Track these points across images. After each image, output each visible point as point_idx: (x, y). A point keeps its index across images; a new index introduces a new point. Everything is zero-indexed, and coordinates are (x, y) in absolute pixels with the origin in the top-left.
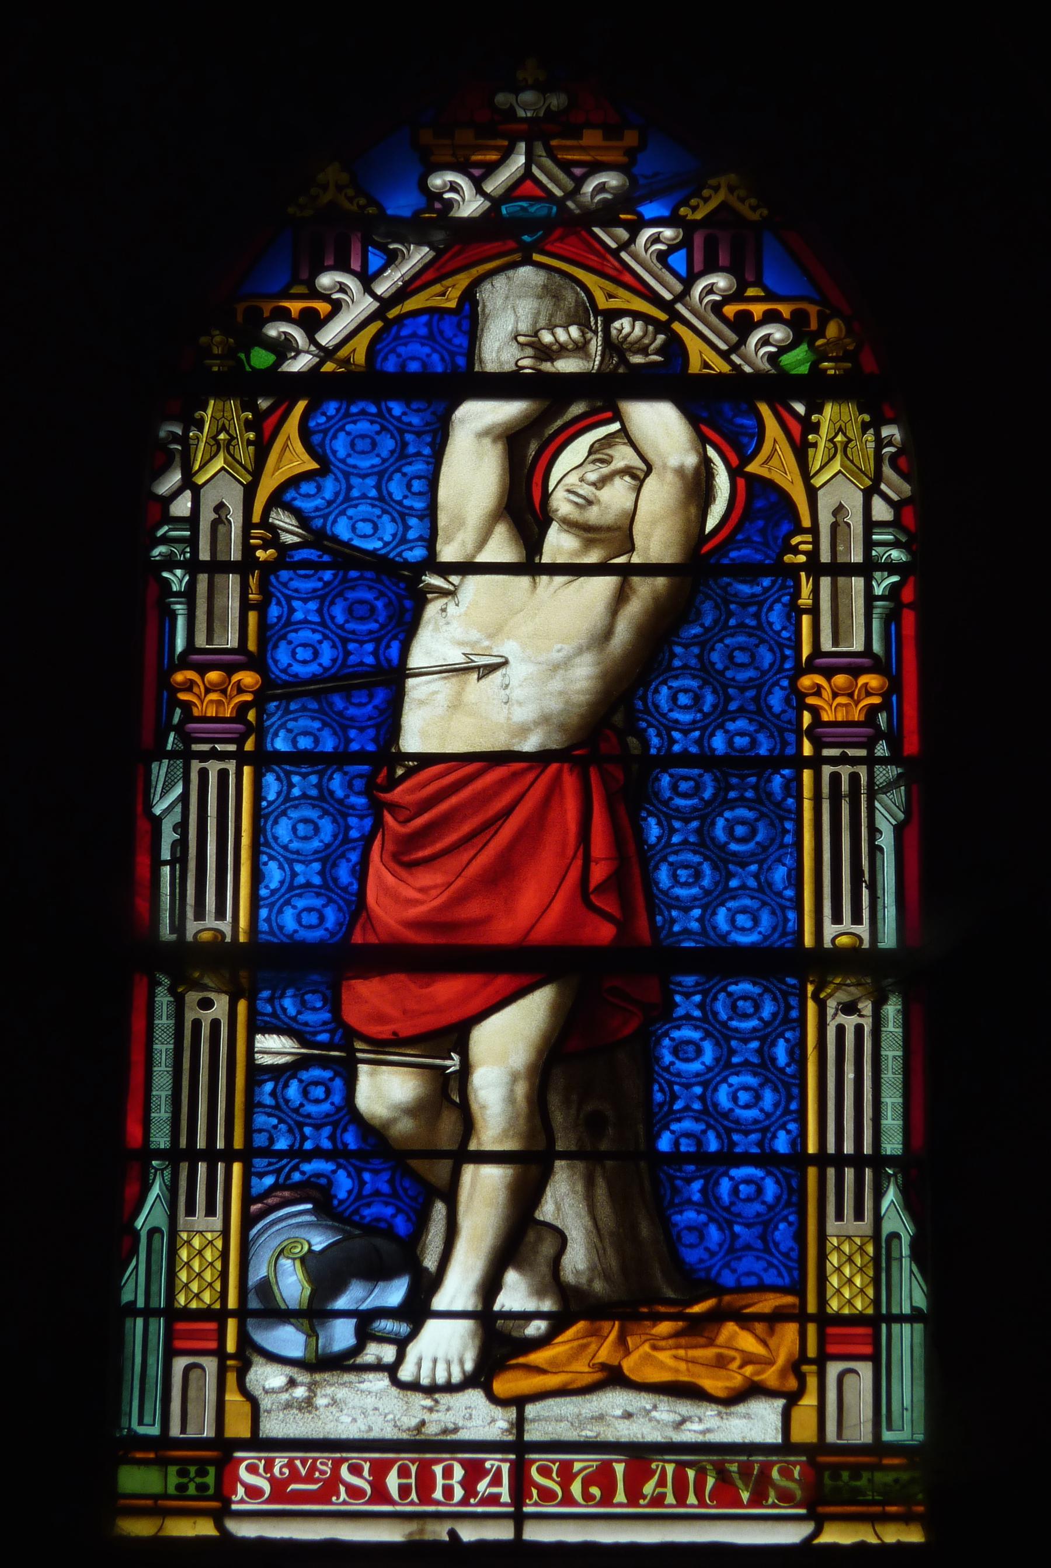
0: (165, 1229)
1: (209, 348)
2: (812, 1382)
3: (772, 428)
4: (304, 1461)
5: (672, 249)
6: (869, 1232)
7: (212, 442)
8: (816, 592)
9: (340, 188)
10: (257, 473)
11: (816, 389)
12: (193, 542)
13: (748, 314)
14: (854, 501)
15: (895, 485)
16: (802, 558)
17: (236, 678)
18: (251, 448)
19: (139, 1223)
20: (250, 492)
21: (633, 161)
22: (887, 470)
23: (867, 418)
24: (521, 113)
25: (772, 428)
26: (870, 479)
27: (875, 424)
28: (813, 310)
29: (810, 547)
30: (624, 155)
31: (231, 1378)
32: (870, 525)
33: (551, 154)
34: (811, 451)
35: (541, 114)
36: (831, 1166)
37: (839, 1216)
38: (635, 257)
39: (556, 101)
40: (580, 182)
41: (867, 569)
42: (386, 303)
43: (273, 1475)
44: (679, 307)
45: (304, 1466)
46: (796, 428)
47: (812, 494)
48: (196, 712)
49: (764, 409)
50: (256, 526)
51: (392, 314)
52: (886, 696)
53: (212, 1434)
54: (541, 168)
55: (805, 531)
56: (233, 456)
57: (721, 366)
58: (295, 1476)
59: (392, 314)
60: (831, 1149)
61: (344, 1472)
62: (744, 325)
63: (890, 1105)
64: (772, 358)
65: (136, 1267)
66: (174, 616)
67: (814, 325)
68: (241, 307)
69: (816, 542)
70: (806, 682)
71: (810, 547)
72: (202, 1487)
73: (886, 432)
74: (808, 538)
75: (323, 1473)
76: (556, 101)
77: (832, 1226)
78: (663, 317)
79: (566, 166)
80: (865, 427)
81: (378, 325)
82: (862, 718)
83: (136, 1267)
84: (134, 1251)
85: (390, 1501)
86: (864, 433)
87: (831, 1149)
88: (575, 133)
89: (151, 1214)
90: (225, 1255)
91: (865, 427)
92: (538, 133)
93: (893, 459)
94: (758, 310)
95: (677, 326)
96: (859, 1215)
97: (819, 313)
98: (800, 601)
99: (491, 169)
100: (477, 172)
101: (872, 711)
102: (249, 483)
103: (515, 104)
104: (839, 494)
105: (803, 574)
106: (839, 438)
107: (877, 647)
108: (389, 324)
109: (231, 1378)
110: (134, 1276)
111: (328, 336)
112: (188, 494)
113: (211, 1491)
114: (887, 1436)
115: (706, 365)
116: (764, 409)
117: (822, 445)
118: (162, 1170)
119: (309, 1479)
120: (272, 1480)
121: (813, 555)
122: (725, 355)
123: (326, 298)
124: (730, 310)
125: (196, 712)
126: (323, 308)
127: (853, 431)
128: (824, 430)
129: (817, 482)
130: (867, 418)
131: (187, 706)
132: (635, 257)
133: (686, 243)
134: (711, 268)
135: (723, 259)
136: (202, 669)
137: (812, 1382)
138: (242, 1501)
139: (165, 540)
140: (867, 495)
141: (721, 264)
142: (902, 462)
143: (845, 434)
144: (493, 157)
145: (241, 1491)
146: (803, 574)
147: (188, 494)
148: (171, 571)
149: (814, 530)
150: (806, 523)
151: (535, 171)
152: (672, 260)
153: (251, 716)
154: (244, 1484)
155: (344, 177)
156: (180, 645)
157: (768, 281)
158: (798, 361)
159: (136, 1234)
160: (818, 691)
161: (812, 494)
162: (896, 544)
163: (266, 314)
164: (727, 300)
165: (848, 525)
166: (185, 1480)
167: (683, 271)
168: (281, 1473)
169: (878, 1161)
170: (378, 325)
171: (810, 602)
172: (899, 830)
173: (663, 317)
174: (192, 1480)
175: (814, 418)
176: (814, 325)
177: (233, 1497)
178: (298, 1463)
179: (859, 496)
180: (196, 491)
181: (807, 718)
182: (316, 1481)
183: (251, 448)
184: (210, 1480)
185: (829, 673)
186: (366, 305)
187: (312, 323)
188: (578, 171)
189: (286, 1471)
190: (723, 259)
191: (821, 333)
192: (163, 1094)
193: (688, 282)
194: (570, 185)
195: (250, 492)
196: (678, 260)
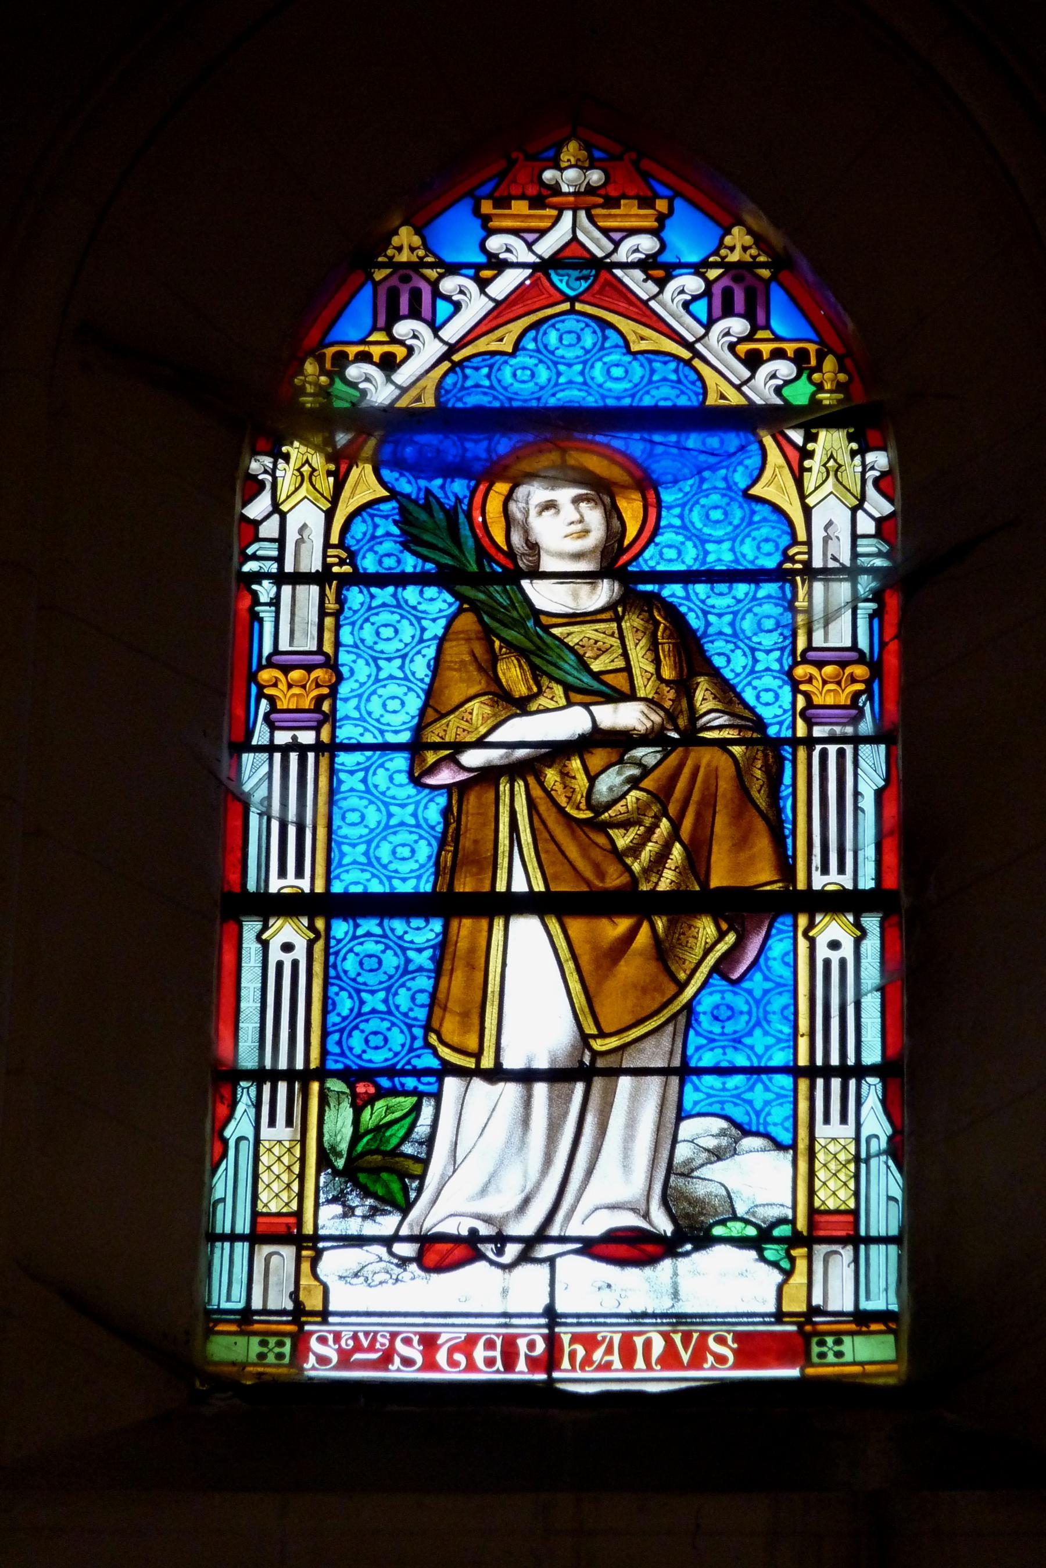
0: (251, 1138)
1: (302, 388)
2: (801, 1265)
3: (774, 456)
4: (366, 1334)
5: (695, 298)
6: (852, 1134)
7: (297, 473)
8: (810, 594)
9: (412, 249)
10: (335, 500)
11: (814, 419)
12: (280, 559)
13: (758, 353)
14: (842, 517)
15: (879, 505)
16: (799, 566)
17: (313, 675)
18: (331, 479)
19: (227, 1133)
20: (330, 515)
21: (662, 227)
22: (871, 491)
23: (854, 446)
24: (565, 189)
25: (774, 456)
26: (856, 498)
27: (862, 451)
28: (812, 348)
29: (806, 557)
30: (656, 220)
31: (306, 1267)
32: (855, 537)
33: (591, 218)
34: (806, 474)
35: (582, 190)
36: (820, 1077)
37: (827, 1120)
38: (664, 306)
39: (596, 177)
40: (617, 244)
41: (851, 573)
42: (453, 348)
43: (340, 1346)
44: (699, 346)
45: (366, 1338)
46: (793, 455)
47: (807, 511)
48: (279, 706)
49: (768, 441)
50: (334, 546)
51: (457, 357)
52: (868, 682)
53: (311, 1232)
54: (586, 233)
55: (802, 543)
56: (314, 486)
57: (735, 399)
58: (358, 1348)
59: (457, 357)
60: (819, 1062)
61: (399, 1345)
62: (753, 361)
63: (869, 1025)
64: (778, 390)
65: (226, 1169)
66: (261, 621)
67: (813, 363)
68: (330, 351)
69: (810, 553)
70: (800, 671)
71: (806, 557)
72: (280, 1356)
73: (871, 457)
74: (804, 549)
75: (382, 1345)
76: (596, 177)
77: (821, 1130)
78: (686, 354)
79: (605, 232)
80: (853, 454)
81: (446, 365)
82: (849, 703)
83: (226, 1169)
84: (224, 1155)
85: (440, 1370)
86: (852, 459)
87: (819, 1062)
88: (612, 202)
89: (240, 1126)
90: (303, 1160)
91: (853, 454)
92: (587, 201)
93: (876, 482)
94: (766, 348)
95: (697, 363)
96: (844, 1120)
97: (818, 351)
98: (797, 604)
99: (543, 232)
100: (530, 237)
101: (856, 695)
102: (328, 510)
103: (560, 182)
104: (831, 512)
105: (798, 579)
106: (831, 463)
107: (863, 644)
108: (455, 365)
109: (306, 1267)
110: (224, 1176)
111: (404, 375)
112: (276, 518)
113: (287, 1360)
114: (865, 1305)
115: (723, 397)
116: (768, 441)
117: (815, 470)
118: (248, 1088)
119: (371, 1348)
120: (340, 1351)
121: (807, 564)
122: (738, 388)
123: (402, 343)
124: (742, 349)
125: (279, 706)
126: (400, 352)
127: (844, 458)
128: (817, 456)
129: (810, 501)
130: (854, 446)
131: (272, 700)
132: (664, 306)
133: (707, 293)
134: (728, 311)
135: (739, 304)
136: (286, 669)
137: (801, 1265)
138: (313, 1368)
139: (255, 557)
140: (854, 510)
141: (736, 311)
142: (882, 484)
143: (835, 461)
144: (546, 224)
145: (312, 1359)
146: (798, 579)
147: (276, 518)
148: (260, 584)
149: (809, 543)
150: (802, 536)
151: (581, 236)
152: (693, 307)
153: (326, 707)
154: (315, 1354)
155: (416, 240)
156: (267, 649)
157: (774, 324)
158: (800, 394)
159: (225, 1142)
160: (810, 680)
161: (807, 511)
162: (879, 554)
163: (351, 357)
164: (741, 340)
165: (838, 538)
166: (265, 1350)
167: (704, 318)
168: (347, 1345)
169: (860, 1071)
170: (446, 365)
171: (806, 604)
172: (879, 794)
173: (686, 354)
174: (271, 1350)
175: (810, 446)
176: (813, 363)
177: (305, 1365)
178: (361, 1336)
179: (849, 513)
180: (283, 516)
181: (801, 702)
182: (378, 1351)
183: (331, 479)
184: (287, 1349)
185: (820, 664)
186: (436, 349)
187: (389, 364)
188: (616, 236)
189: (351, 1343)
190: (739, 304)
191: (819, 368)
192: (251, 1026)
193: (708, 326)
194: (610, 247)
195: (330, 515)
196: (700, 308)
